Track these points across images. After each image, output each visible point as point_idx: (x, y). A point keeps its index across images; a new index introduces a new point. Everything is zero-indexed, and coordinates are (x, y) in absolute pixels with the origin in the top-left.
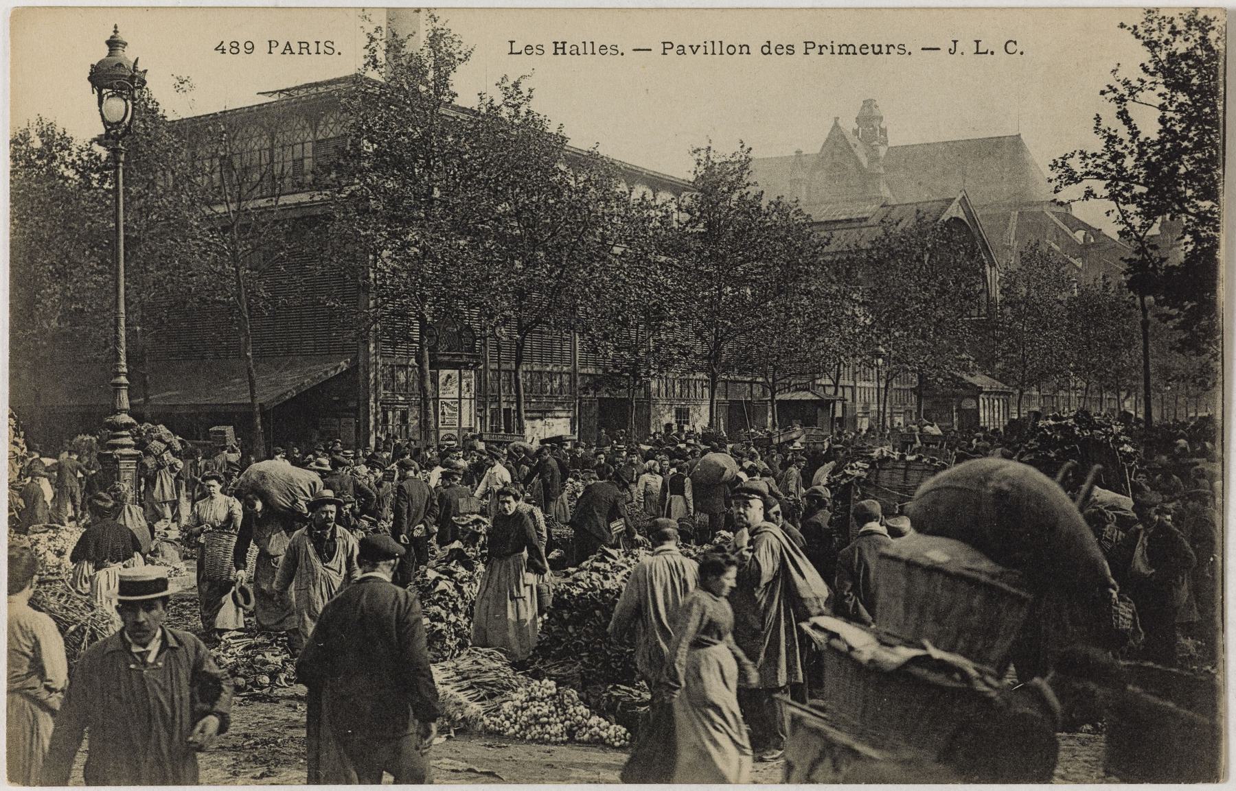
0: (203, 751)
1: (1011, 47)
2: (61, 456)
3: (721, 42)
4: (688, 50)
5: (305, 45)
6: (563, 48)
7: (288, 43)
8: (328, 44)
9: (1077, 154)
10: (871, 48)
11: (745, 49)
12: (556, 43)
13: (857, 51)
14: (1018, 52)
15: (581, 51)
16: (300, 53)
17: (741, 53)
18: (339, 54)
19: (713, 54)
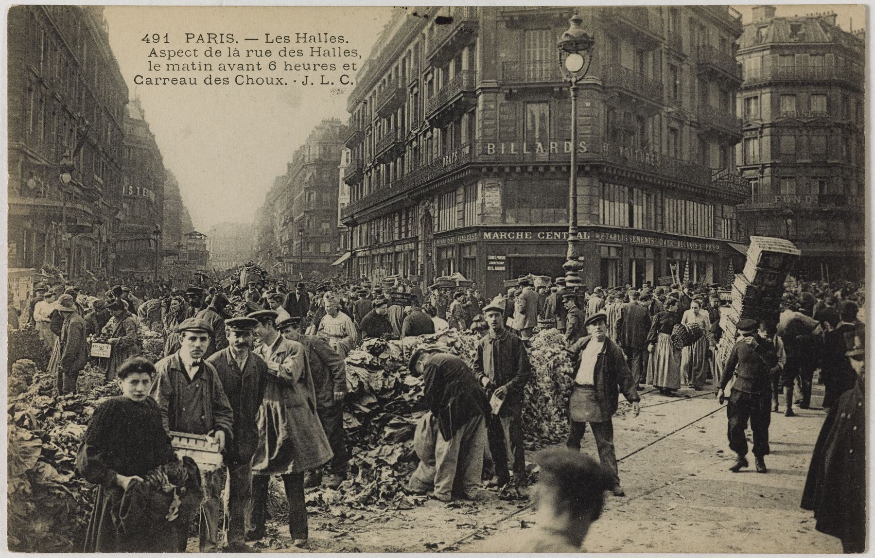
1: (139, 80)
4: (227, 67)
7: (201, 35)
8: (229, 36)
9: (268, 545)
10: (302, 66)
11: (208, 67)
13: (293, 68)
14: (350, 83)
15: (331, 54)
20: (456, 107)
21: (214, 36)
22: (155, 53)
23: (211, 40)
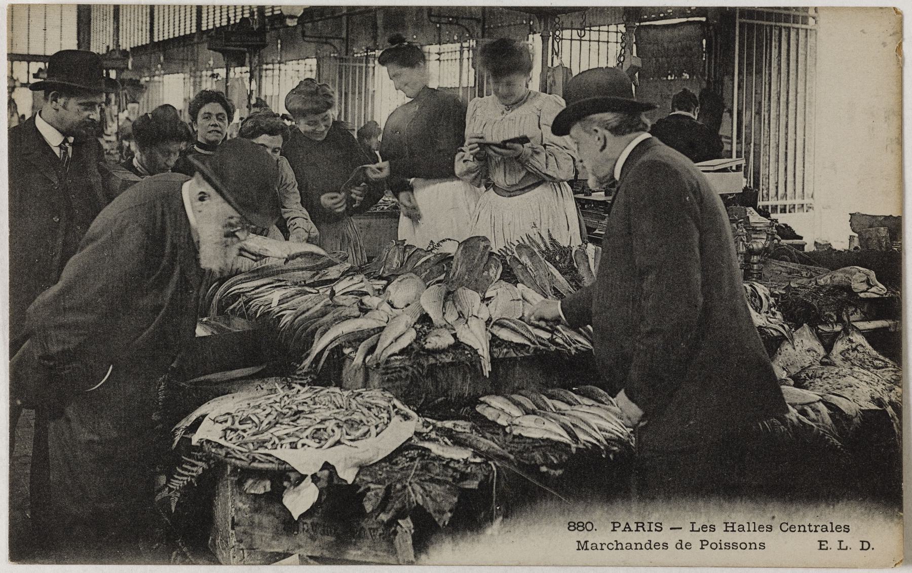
5: (641, 525)
6: (733, 527)
7: (627, 524)
15: (746, 529)
17: (750, 549)
19: (749, 531)
21: (641, 525)
22: (629, 528)
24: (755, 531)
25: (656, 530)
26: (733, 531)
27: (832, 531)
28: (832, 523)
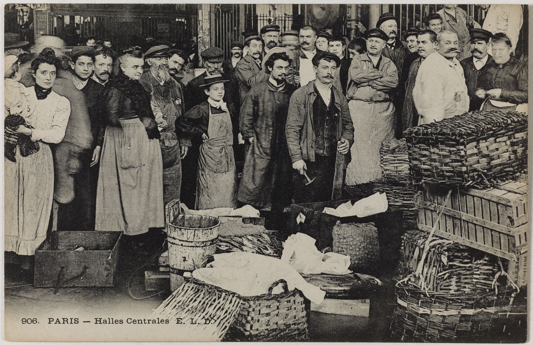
0: (157, 207)
2: (78, 33)
3: (112, 319)
5: (66, 320)
6: (100, 321)
7: (58, 319)
8: (76, 320)
12: (96, 319)
15: (108, 322)
16: (64, 323)
18: (199, 324)
19: (109, 323)
20: (310, 338)
21: (66, 320)
22: (59, 321)
23: (65, 322)
24: (113, 323)
25: (75, 323)
26: (100, 323)
27: (159, 323)
28: (158, 319)
